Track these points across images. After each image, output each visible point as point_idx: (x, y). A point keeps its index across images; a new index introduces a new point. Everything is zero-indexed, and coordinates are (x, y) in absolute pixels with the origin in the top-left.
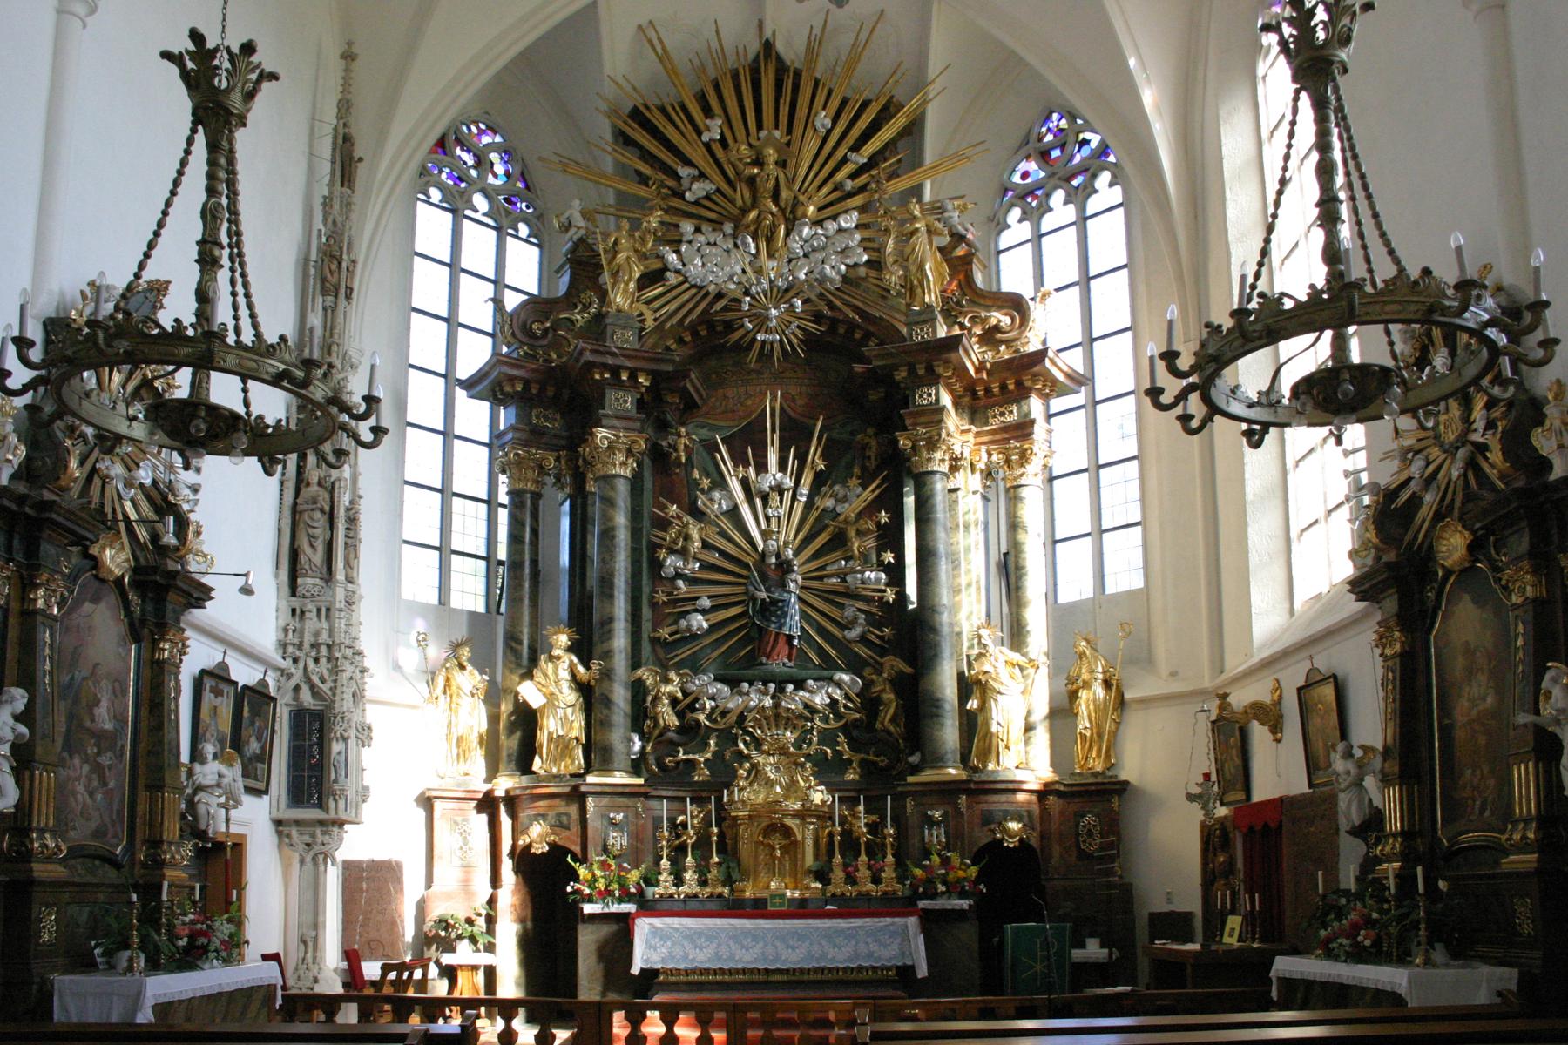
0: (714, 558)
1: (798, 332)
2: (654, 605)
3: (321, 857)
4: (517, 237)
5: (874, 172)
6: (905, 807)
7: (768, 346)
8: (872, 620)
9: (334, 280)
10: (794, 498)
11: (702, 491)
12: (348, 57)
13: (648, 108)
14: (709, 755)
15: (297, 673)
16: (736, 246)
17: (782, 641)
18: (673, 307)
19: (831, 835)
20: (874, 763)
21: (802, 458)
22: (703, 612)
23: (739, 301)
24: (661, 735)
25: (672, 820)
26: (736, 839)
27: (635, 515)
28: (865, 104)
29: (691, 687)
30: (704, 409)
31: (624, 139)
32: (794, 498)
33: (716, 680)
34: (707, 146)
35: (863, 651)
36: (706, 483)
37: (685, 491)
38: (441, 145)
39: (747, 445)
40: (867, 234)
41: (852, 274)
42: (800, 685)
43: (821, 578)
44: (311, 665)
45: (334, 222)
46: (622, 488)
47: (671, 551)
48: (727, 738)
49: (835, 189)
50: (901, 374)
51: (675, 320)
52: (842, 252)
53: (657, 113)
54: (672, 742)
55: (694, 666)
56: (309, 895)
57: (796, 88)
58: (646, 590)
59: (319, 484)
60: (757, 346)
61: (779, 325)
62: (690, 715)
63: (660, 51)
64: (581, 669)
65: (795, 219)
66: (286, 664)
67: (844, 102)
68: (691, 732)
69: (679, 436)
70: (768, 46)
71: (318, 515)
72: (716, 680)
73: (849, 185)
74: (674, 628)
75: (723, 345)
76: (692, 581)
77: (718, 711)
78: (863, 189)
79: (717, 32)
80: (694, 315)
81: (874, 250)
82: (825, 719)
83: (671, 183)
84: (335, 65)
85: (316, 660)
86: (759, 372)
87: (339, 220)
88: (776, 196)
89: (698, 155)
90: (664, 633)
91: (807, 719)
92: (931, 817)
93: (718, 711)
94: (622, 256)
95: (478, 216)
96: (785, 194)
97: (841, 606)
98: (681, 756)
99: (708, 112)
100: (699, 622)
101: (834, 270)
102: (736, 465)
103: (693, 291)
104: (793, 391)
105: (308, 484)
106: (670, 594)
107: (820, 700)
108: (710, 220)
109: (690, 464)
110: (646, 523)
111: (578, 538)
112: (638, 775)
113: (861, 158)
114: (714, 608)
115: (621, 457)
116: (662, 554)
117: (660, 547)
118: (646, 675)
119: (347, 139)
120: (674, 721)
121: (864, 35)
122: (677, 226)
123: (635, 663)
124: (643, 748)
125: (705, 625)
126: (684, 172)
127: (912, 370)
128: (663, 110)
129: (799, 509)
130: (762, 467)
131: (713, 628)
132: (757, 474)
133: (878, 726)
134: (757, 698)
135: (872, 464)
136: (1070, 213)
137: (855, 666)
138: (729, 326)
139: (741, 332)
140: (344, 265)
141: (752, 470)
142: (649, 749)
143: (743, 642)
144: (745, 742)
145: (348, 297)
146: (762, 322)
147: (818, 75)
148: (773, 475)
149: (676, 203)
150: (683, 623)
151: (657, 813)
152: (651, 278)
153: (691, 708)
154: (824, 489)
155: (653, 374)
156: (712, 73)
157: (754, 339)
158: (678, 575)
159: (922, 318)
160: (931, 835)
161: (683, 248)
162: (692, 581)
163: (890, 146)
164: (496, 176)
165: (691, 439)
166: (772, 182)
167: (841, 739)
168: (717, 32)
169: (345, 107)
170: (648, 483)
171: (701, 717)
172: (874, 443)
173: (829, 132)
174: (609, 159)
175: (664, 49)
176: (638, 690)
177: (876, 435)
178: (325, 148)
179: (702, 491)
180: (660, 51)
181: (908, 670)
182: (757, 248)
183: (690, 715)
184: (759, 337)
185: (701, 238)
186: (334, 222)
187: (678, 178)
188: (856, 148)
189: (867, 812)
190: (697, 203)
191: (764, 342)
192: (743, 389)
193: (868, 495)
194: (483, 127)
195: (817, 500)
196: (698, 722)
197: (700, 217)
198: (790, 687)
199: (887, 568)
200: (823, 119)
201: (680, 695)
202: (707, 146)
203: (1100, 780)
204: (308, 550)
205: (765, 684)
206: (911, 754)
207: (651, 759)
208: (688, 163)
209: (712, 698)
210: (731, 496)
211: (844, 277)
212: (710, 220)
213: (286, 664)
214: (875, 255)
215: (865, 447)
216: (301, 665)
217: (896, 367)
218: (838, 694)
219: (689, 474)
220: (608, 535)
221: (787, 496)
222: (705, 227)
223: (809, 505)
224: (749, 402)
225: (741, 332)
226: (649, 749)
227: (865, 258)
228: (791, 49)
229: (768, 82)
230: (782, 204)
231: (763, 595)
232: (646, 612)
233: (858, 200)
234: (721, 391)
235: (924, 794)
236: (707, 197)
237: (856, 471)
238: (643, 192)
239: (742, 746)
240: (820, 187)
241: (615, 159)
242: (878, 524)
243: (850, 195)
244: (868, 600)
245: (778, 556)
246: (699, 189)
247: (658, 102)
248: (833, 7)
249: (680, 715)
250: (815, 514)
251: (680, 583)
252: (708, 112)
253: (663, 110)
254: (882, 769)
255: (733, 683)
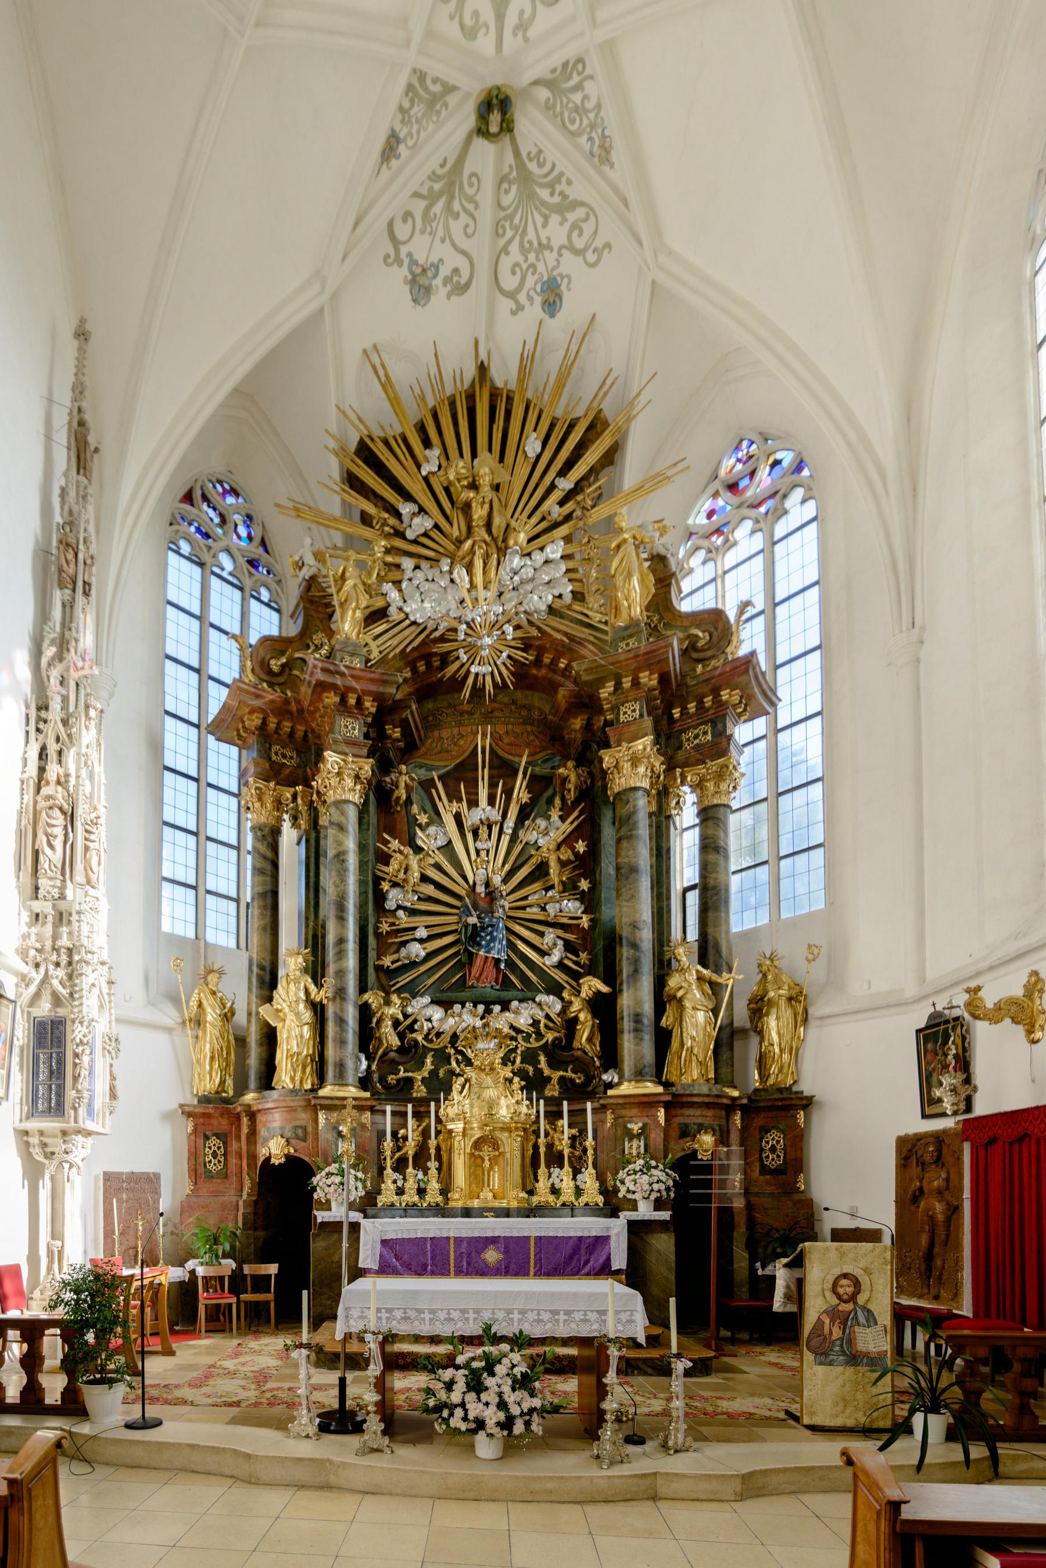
0: (429, 890)
1: (509, 663)
2: (378, 935)
3: (66, 1166)
4: (259, 600)
5: (579, 498)
6: (742, 1119)
7: (480, 678)
8: (569, 946)
9: (71, 570)
10: (501, 832)
11: (420, 826)
12: (82, 335)
13: (372, 440)
14: (426, 1074)
15: (37, 977)
16: (452, 581)
17: (490, 964)
18: (395, 641)
19: (536, 1147)
20: (572, 1080)
21: (508, 793)
22: (421, 941)
23: (455, 630)
24: (385, 1054)
25: (394, 1134)
26: (450, 1151)
27: (362, 848)
28: (571, 426)
29: (410, 1010)
30: (422, 750)
31: (352, 481)
32: (501, 832)
33: (432, 1002)
34: (426, 479)
35: (559, 976)
36: (423, 819)
37: (405, 828)
38: (188, 498)
39: (460, 778)
40: (571, 564)
41: (558, 604)
42: (505, 1007)
43: (524, 908)
44: (51, 967)
45: (71, 512)
46: (352, 813)
47: (395, 885)
48: (442, 1057)
49: (543, 519)
50: (606, 691)
51: (398, 650)
52: (549, 583)
53: (381, 445)
54: (393, 1061)
55: (412, 991)
56: (57, 1206)
57: (508, 413)
58: (372, 920)
59: (58, 783)
60: (470, 681)
61: (487, 661)
62: (410, 1036)
63: (383, 379)
64: (312, 988)
65: (507, 548)
66: (25, 969)
67: (552, 426)
68: (411, 1052)
69: (400, 773)
70: (483, 369)
71: (57, 813)
72: (432, 1002)
73: (557, 512)
74: (395, 956)
75: (440, 680)
76: (412, 912)
77: (434, 1032)
78: (568, 518)
79: (436, 355)
80: (415, 644)
81: (576, 580)
82: (527, 1038)
83: (393, 521)
84: (70, 346)
85: (57, 965)
86: (471, 713)
87: (75, 508)
88: (488, 525)
89: (416, 488)
90: (387, 961)
91: (512, 1038)
92: (630, 1130)
93: (434, 1032)
94: (350, 583)
95: (225, 574)
96: (498, 521)
97: (542, 934)
98: (402, 1074)
99: (427, 444)
100: (417, 950)
101: (538, 602)
102: (450, 801)
103: (413, 628)
104: (501, 730)
105: (48, 783)
106: (393, 924)
107: (523, 1021)
108: (427, 559)
109: (409, 801)
110: (371, 857)
111: (312, 874)
112: (365, 1089)
113: (565, 484)
114: (431, 938)
115: (349, 782)
116: (385, 886)
117: (384, 880)
118: (373, 998)
119: (81, 423)
120: (395, 1042)
121: (574, 348)
122: (398, 566)
123: (363, 989)
124: (369, 1067)
125: (423, 954)
126: (406, 509)
127: (618, 686)
128: (386, 442)
129: (505, 840)
130: (473, 803)
131: (430, 956)
132: (469, 808)
133: (576, 1044)
134: (467, 1018)
135: (571, 796)
136: (758, 541)
137: (555, 989)
138: (445, 659)
139: (457, 664)
140: (81, 556)
141: (465, 803)
142: (374, 1067)
143: (460, 966)
144: (458, 1062)
145: (86, 594)
146: (473, 650)
147: (529, 395)
148: (484, 811)
149: (398, 543)
150: (403, 952)
151: (380, 1127)
152: (376, 616)
153: (411, 1028)
154: (527, 823)
155: (379, 698)
156: (431, 403)
157: (468, 672)
158: (399, 907)
159: (629, 631)
160: (631, 1147)
161: (404, 585)
162: (412, 912)
163: (593, 472)
164: (239, 537)
165: (412, 779)
166: (487, 506)
167: (542, 1058)
168: (436, 355)
169: (79, 390)
170: (372, 808)
171: (420, 1038)
172: (573, 778)
173: (539, 457)
174: (336, 500)
175: (387, 375)
176: (365, 1012)
177: (576, 767)
178: (62, 437)
179: (420, 826)
180: (383, 379)
181: (605, 989)
182: (502, 1185)
183: (410, 1036)
184: (474, 669)
185: (419, 574)
186: (71, 512)
187: (398, 515)
188: (563, 473)
189: (570, 1126)
190: (415, 542)
191: (477, 675)
192: (456, 731)
193: (567, 827)
194: (227, 487)
195: (521, 833)
196: (416, 1041)
197: (419, 556)
198: (497, 1008)
199: (583, 897)
200: (533, 446)
201: (401, 1017)
202: (426, 479)
203: (785, 1095)
204: (47, 850)
205: (475, 1006)
206: (606, 1071)
207: (376, 1077)
208: (408, 497)
209: (429, 1020)
210: (445, 833)
211: (550, 607)
212: (427, 559)
213: (25, 969)
214: (578, 587)
215: (565, 780)
216: (42, 970)
217: (600, 682)
218: (540, 1015)
219: (408, 811)
220: (341, 1021)
221: (495, 830)
222: (424, 565)
223: (514, 839)
224: (461, 742)
225: (457, 664)
226: (374, 1067)
227: (570, 588)
228: (504, 375)
229: (481, 410)
230: (494, 531)
231: (473, 920)
232: (372, 941)
233: (563, 530)
234: (436, 733)
235: (623, 1106)
236: (425, 535)
237: (558, 802)
238: (367, 533)
239: (454, 1064)
240: (529, 517)
241: (343, 501)
242: (576, 854)
243: (556, 525)
244: (564, 927)
245: (487, 884)
246: (420, 525)
247: (382, 435)
248: (546, 317)
249: (401, 1036)
250: (520, 847)
251: (401, 913)
252: (427, 444)
253: (386, 442)
254: (578, 1085)
255: (446, 1005)
